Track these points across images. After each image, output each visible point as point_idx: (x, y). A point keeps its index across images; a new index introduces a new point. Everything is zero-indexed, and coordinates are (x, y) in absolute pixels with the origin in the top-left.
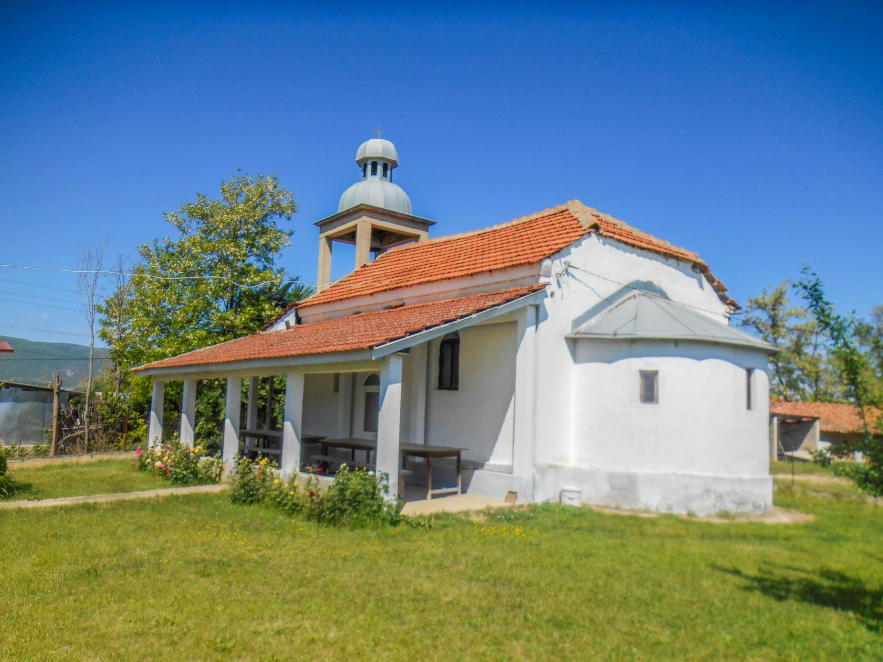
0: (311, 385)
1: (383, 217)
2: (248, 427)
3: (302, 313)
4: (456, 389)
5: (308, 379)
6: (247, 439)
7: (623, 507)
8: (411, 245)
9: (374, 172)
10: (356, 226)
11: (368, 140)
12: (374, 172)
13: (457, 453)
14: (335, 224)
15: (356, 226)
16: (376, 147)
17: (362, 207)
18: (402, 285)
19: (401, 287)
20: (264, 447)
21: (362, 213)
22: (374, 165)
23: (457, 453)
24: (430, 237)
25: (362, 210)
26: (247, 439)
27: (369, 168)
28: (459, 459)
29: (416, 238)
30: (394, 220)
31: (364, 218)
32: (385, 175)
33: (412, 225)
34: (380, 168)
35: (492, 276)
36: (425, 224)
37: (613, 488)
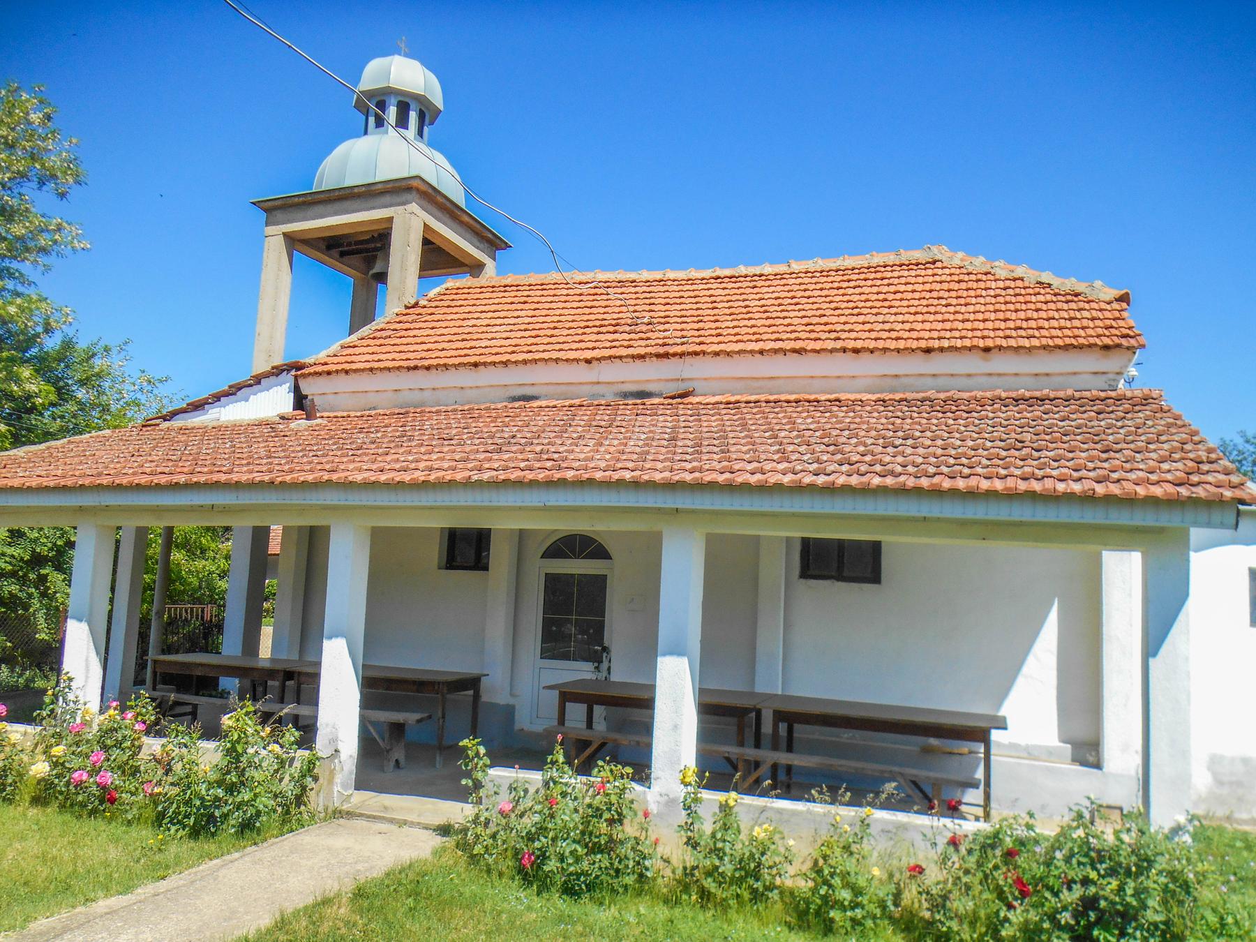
0: (386, 551)
1: (439, 214)
2: (265, 650)
3: (307, 388)
4: (486, 568)
5: (713, 544)
6: (599, 710)
7: (1237, 815)
8: (466, 281)
9: (402, 122)
10: (390, 220)
11: (392, 54)
12: (402, 122)
13: (472, 683)
14: (347, 204)
15: (390, 220)
16: (406, 73)
17: (415, 183)
18: (672, 350)
19: (704, 353)
20: (775, 747)
21: (408, 196)
22: (403, 109)
23: (472, 683)
24: (500, 271)
25: (409, 189)
26: (599, 710)
27: (392, 112)
28: (477, 696)
29: (476, 268)
30: (455, 226)
31: (414, 207)
32: (420, 133)
33: (475, 240)
34: (413, 116)
35: (986, 360)
36: (494, 244)
37: (1219, 782)
